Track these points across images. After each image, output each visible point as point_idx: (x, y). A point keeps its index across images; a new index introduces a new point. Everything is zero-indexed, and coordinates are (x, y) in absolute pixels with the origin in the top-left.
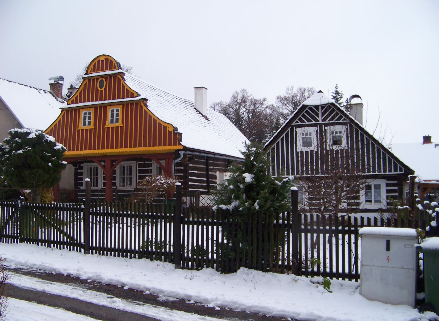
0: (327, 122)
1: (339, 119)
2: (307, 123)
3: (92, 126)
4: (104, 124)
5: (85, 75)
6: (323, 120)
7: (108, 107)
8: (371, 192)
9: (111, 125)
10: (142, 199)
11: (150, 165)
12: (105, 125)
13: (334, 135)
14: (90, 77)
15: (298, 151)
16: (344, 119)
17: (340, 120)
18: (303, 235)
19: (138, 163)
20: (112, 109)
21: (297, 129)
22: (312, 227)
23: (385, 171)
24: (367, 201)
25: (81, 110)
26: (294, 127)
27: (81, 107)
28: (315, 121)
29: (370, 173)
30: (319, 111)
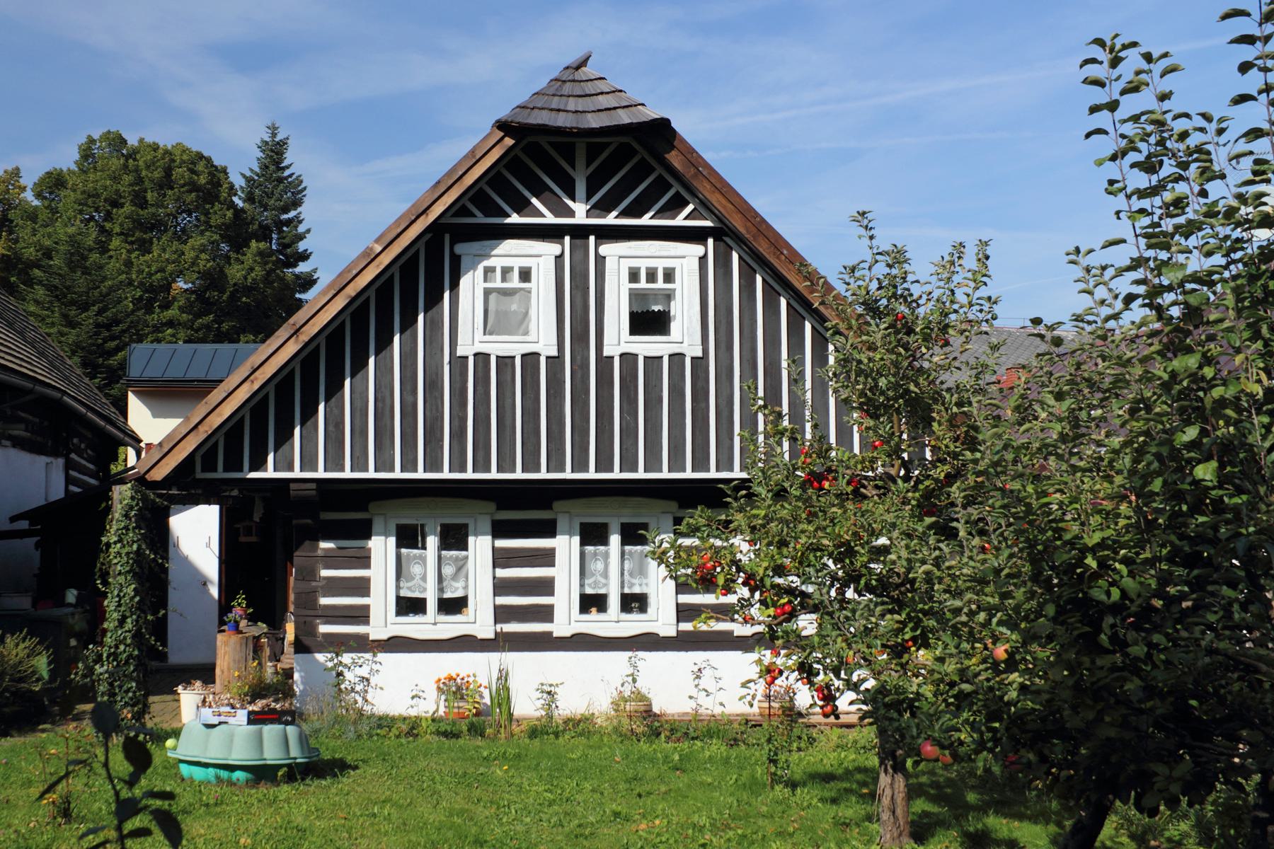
0: (611, 219)
8: (606, 556)
13: (643, 284)
15: (460, 352)
17: (640, 215)
21: (605, 249)
26: (447, 238)
28: (557, 214)
30: (574, 167)
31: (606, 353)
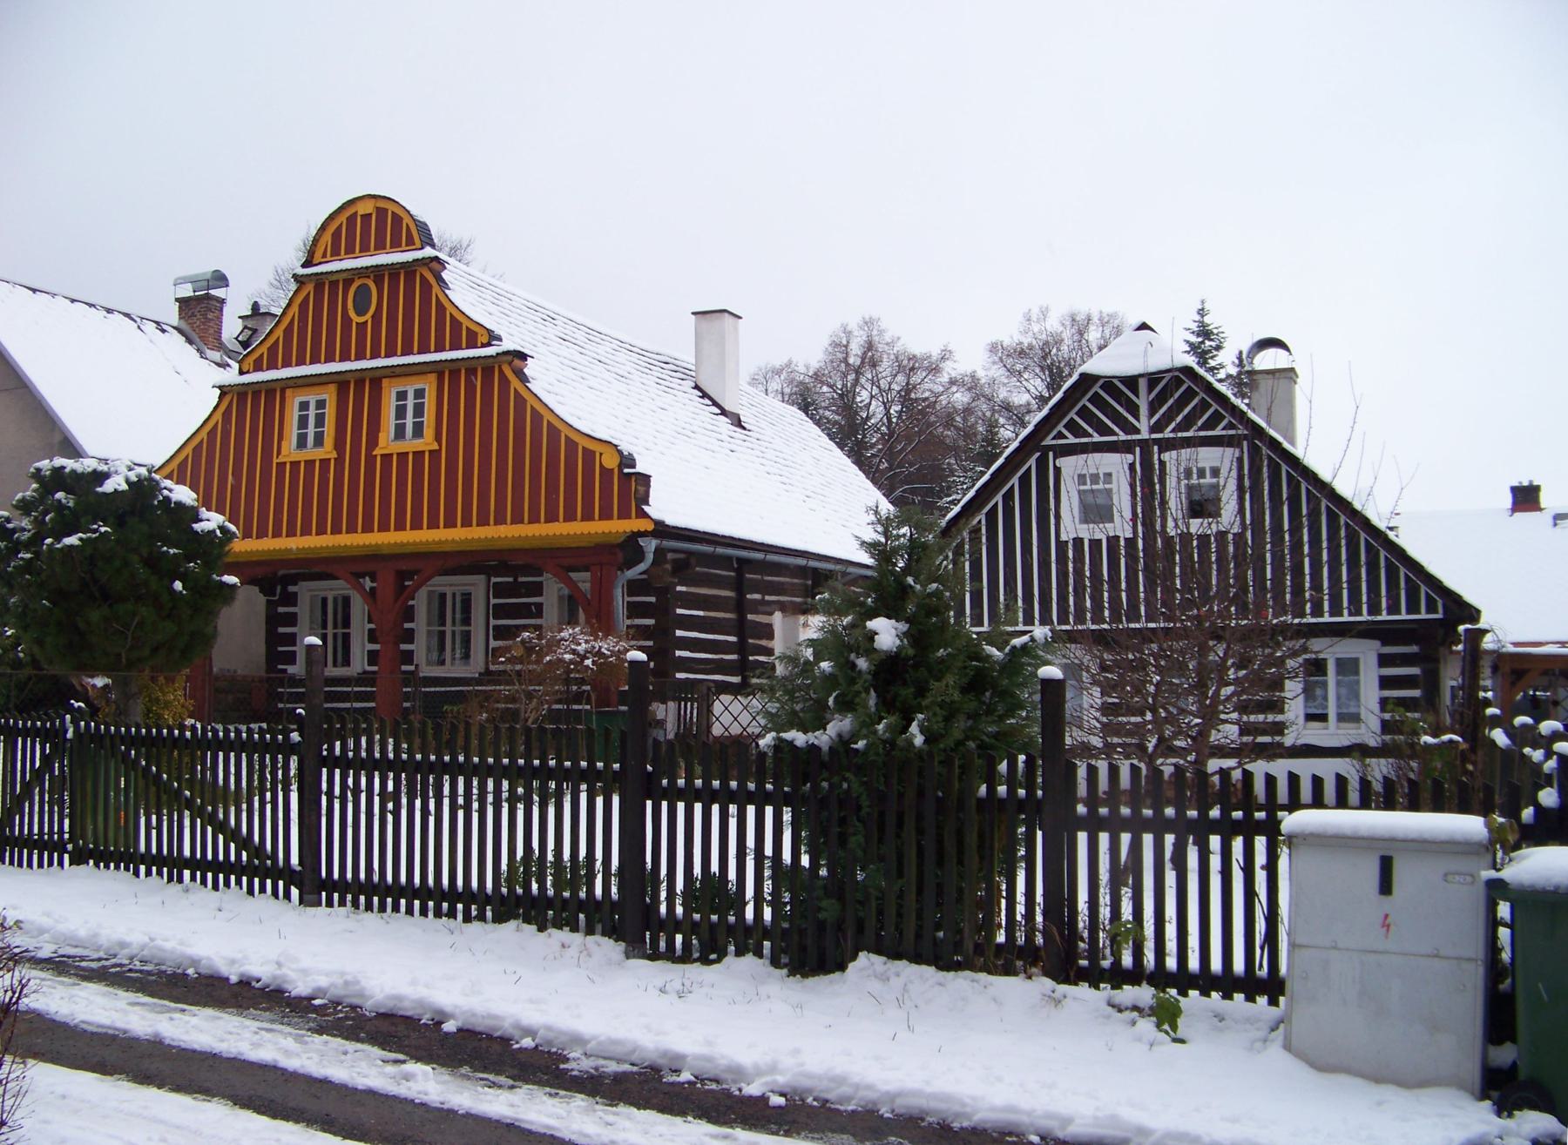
0: (1167, 434)
1: (1209, 425)
2: (1097, 438)
3: (328, 451)
4: (373, 441)
5: (304, 266)
6: (1154, 429)
7: (385, 382)
8: (1324, 685)
9: (397, 447)
10: (508, 708)
11: (537, 589)
12: (377, 445)
13: (1194, 481)
14: (322, 273)
15: (1064, 537)
16: (1230, 426)
17: (1213, 429)
18: (1082, 837)
19: (494, 580)
20: (401, 389)
21: (1061, 462)
22: (1114, 811)
23: (1374, 609)
24: (1310, 717)
25: (289, 392)
26: (1051, 454)
27: (291, 383)
28: (1127, 433)
29: (1322, 616)
30: (1138, 397)
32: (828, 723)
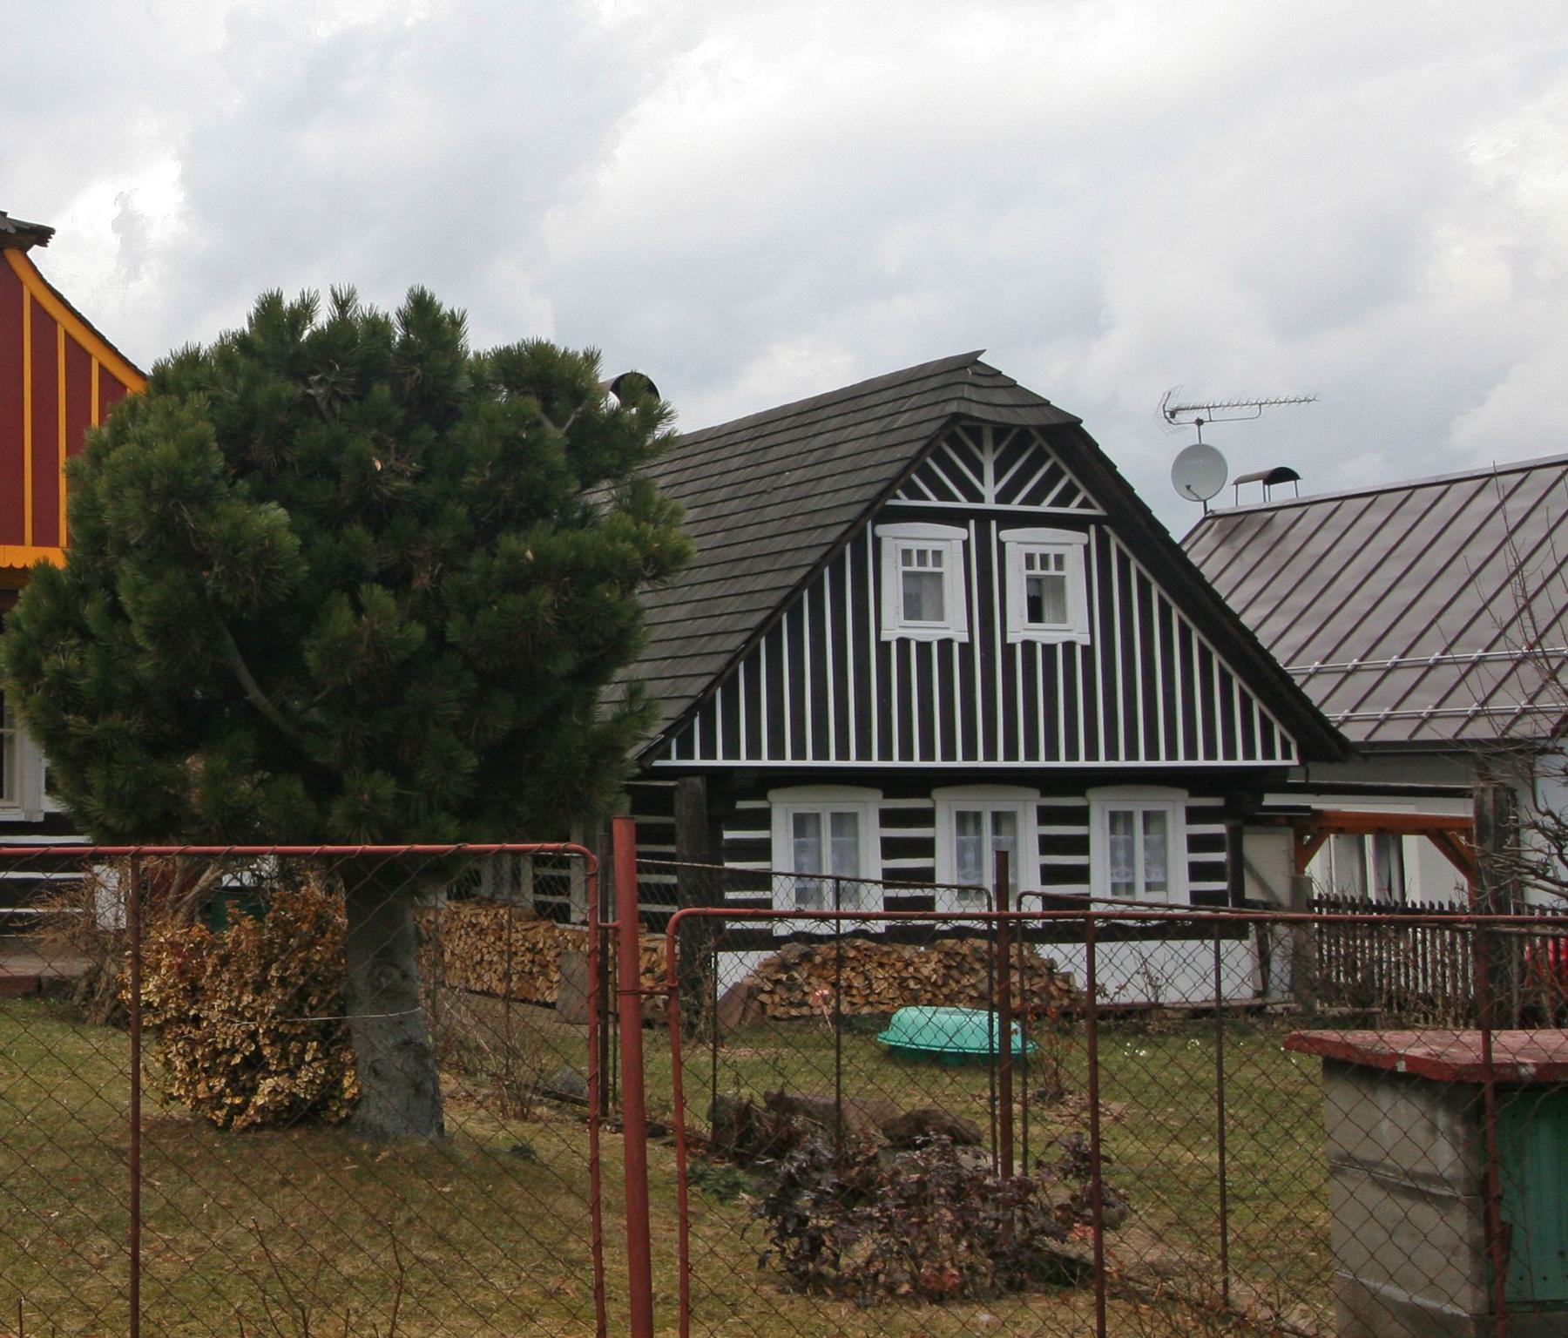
0: (1015, 506)
1: (1063, 500)
2: (934, 502)
6: (1004, 497)
13: (1038, 571)
16: (1085, 504)
17: (1066, 505)
21: (1006, 535)
28: (940, 499)
30: (982, 451)
31: (1009, 641)
32: (396, 596)
